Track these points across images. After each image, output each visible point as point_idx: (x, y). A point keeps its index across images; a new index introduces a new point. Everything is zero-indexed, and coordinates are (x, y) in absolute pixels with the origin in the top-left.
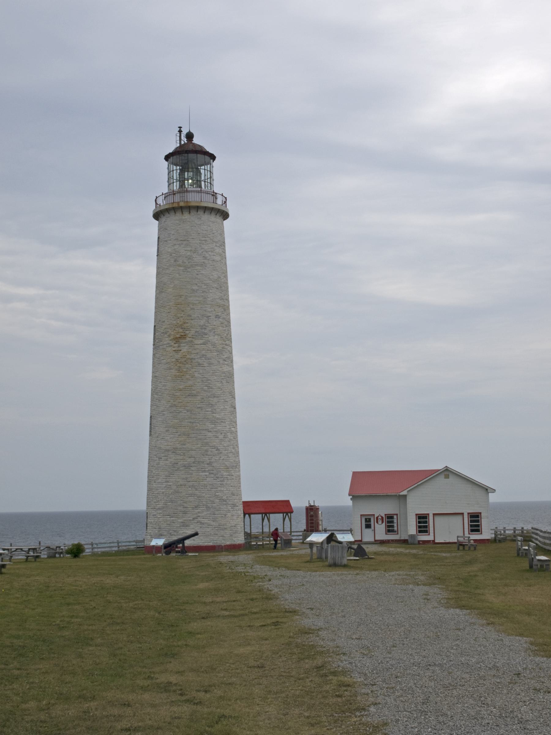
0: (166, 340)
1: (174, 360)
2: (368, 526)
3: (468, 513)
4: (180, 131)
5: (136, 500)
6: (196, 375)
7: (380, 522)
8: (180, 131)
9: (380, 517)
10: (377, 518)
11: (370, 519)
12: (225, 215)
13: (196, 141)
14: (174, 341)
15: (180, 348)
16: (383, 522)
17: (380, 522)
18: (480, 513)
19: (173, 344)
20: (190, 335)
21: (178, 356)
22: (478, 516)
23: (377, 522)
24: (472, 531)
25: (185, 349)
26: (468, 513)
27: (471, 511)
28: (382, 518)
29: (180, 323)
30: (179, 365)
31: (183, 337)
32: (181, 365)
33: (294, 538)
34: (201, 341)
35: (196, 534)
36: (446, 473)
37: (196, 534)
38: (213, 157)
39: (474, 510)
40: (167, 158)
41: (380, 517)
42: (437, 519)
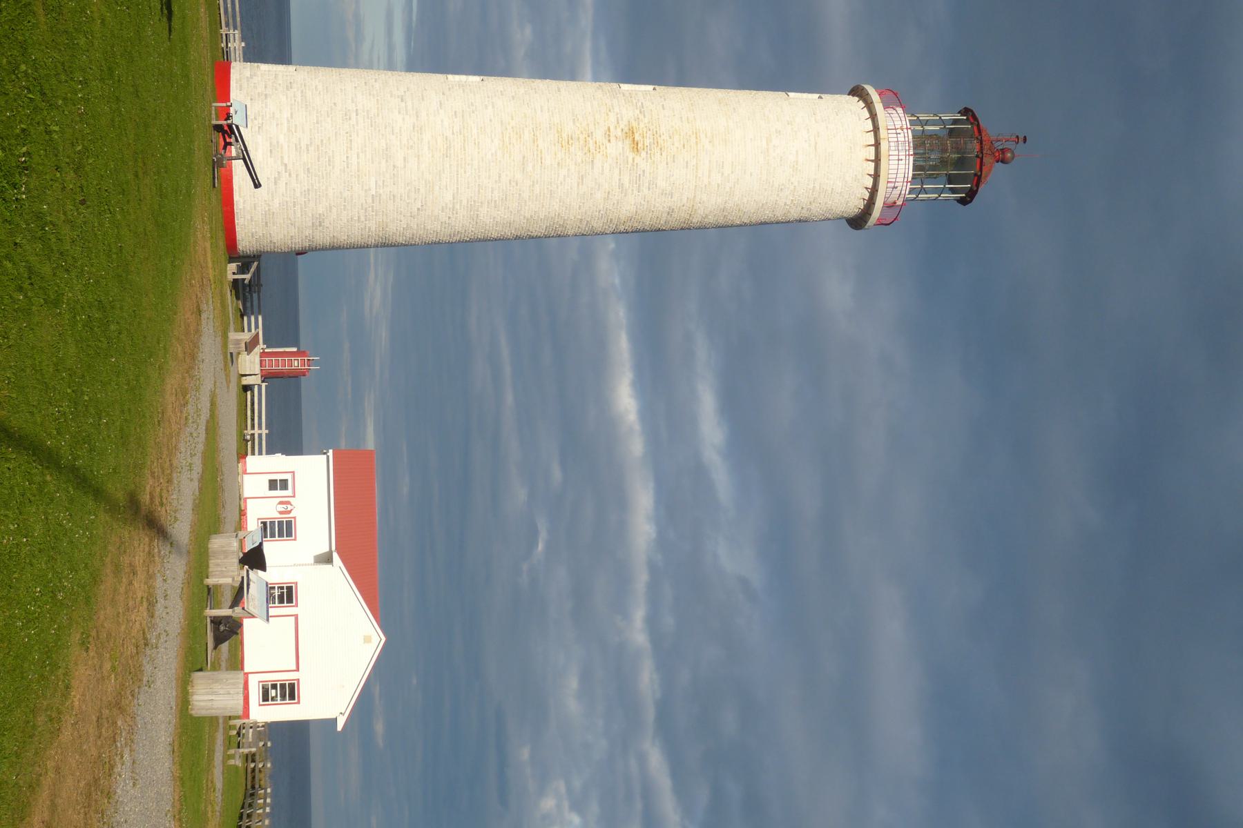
2: (273, 485)
5: (322, 459)
7: (281, 508)
9: (290, 507)
10: (288, 503)
14: (626, 129)
15: (612, 139)
16: (281, 513)
17: (281, 508)
19: (622, 126)
20: (638, 159)
23: (281, 503)
28: (290, 512)
29: (660, 141)
30: (582, 137)
31: (635, 147)
32: (582, 142)
33: (253, 318)
34: (627, 185)
35: (257, 185)
37: (257, 185)
41: (290, 507)
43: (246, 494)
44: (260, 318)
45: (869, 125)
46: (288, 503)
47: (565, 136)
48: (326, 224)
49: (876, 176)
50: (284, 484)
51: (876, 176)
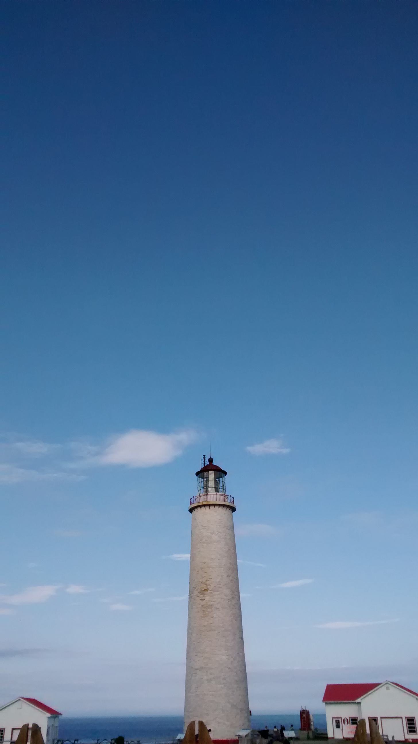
0: (196, 592)
1: (200, 606)
2: (338, 726)
3: (406, 718)
4: (204, 458)
6: (215, 616)
8: (204, 458)
9: (346, 720)
10: (344, 720)
11: (339, 721)
12: (233, 509)
13: (214, 463)
15: (204, 598)
17: (346, 723)
18: (4, 729)
20: (210, 589)
21: (203, 603)
22: (2, 731)
23: (344, 723)
24: (410, 731)
25: (207, 598)
26: (406, 718)
27: (407, 716)
31: (206, 590)
32: (205, 609)
34: (218, 593)
36: (387, 685)
38: (225, 473)
39: (410, 715)
40: (197, 474)
41: (346, 720)
42: (383, 720)
43: (341, 737)
44: (368, 731)
45: (199, 509)
46: (344, 720)
47: (203, 616)
48: (235, 704)
49: (219, 505)
50: (338, 722)
51: (219, 505)
